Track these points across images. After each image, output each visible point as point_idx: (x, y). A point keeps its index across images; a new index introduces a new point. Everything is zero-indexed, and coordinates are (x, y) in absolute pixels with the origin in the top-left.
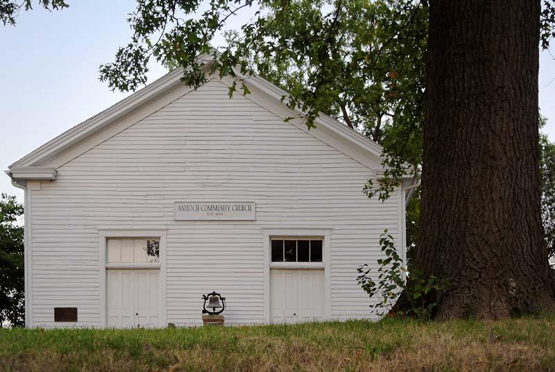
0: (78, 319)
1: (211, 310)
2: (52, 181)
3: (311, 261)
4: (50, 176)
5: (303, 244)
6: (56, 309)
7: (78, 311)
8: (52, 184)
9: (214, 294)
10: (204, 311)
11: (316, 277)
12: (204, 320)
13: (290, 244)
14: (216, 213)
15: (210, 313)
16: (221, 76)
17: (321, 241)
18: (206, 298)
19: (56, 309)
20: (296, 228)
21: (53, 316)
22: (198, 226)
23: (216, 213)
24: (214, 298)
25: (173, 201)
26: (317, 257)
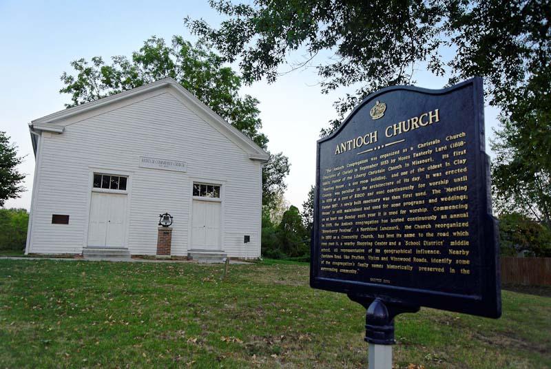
0: (52, 216)
1: (164, 223)
2: (60, 133)
3: (120, 189)
4: (61, 131)
5: (115, 178)
6: (53, 215)
7: (70, 217)
8: (60, 135)
9: (167, 214)
10: (160, 224)
11: (216, 206)
12: (159, 230)
13: (107, 178)
14: (164, 165)
15: (164, 226)
16: (235, 72)
17: (126, 179)
18: (161, 216)
19: (53, 215)
20: (112, 169)
21: (51, 219)
22: (153, 171)
23: (164, 165)
24: (166, 217)
25: (138, 156)
26: (123, 186)
